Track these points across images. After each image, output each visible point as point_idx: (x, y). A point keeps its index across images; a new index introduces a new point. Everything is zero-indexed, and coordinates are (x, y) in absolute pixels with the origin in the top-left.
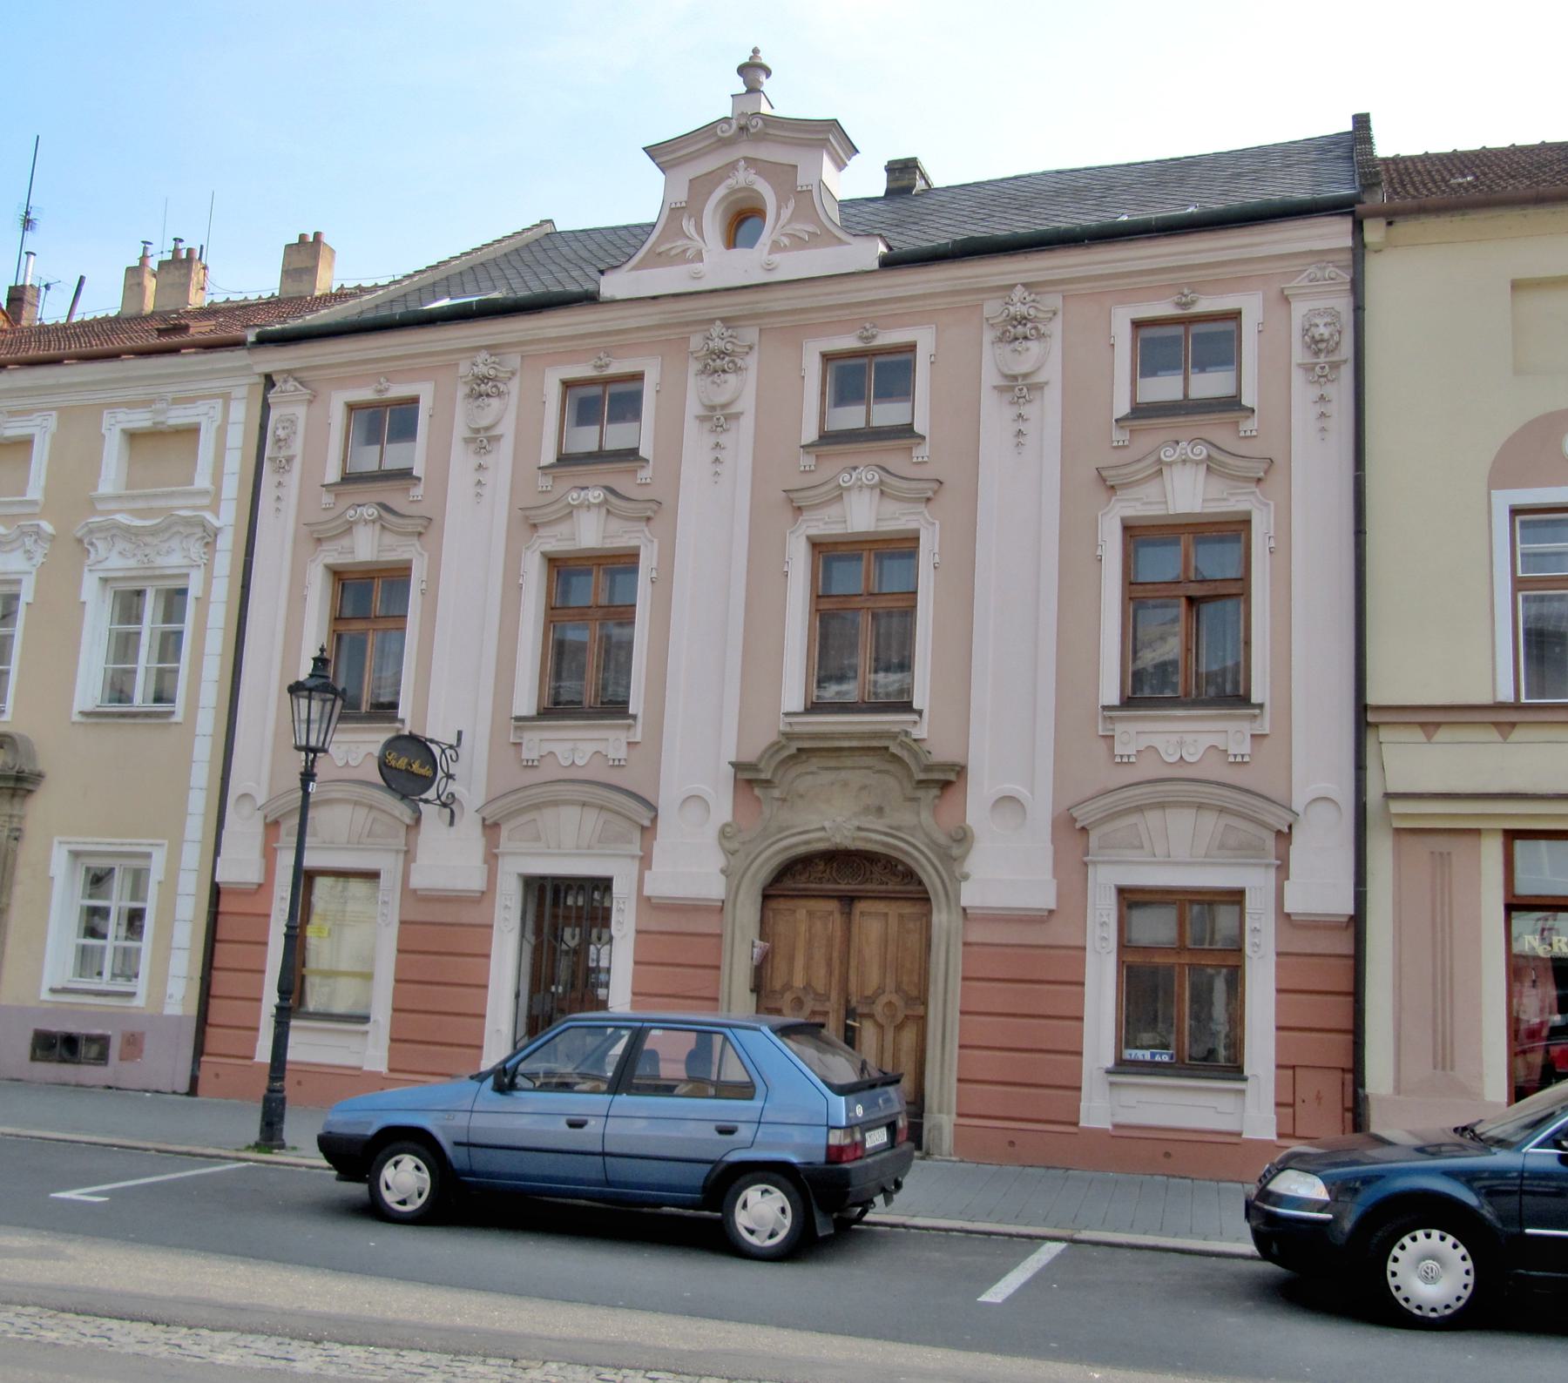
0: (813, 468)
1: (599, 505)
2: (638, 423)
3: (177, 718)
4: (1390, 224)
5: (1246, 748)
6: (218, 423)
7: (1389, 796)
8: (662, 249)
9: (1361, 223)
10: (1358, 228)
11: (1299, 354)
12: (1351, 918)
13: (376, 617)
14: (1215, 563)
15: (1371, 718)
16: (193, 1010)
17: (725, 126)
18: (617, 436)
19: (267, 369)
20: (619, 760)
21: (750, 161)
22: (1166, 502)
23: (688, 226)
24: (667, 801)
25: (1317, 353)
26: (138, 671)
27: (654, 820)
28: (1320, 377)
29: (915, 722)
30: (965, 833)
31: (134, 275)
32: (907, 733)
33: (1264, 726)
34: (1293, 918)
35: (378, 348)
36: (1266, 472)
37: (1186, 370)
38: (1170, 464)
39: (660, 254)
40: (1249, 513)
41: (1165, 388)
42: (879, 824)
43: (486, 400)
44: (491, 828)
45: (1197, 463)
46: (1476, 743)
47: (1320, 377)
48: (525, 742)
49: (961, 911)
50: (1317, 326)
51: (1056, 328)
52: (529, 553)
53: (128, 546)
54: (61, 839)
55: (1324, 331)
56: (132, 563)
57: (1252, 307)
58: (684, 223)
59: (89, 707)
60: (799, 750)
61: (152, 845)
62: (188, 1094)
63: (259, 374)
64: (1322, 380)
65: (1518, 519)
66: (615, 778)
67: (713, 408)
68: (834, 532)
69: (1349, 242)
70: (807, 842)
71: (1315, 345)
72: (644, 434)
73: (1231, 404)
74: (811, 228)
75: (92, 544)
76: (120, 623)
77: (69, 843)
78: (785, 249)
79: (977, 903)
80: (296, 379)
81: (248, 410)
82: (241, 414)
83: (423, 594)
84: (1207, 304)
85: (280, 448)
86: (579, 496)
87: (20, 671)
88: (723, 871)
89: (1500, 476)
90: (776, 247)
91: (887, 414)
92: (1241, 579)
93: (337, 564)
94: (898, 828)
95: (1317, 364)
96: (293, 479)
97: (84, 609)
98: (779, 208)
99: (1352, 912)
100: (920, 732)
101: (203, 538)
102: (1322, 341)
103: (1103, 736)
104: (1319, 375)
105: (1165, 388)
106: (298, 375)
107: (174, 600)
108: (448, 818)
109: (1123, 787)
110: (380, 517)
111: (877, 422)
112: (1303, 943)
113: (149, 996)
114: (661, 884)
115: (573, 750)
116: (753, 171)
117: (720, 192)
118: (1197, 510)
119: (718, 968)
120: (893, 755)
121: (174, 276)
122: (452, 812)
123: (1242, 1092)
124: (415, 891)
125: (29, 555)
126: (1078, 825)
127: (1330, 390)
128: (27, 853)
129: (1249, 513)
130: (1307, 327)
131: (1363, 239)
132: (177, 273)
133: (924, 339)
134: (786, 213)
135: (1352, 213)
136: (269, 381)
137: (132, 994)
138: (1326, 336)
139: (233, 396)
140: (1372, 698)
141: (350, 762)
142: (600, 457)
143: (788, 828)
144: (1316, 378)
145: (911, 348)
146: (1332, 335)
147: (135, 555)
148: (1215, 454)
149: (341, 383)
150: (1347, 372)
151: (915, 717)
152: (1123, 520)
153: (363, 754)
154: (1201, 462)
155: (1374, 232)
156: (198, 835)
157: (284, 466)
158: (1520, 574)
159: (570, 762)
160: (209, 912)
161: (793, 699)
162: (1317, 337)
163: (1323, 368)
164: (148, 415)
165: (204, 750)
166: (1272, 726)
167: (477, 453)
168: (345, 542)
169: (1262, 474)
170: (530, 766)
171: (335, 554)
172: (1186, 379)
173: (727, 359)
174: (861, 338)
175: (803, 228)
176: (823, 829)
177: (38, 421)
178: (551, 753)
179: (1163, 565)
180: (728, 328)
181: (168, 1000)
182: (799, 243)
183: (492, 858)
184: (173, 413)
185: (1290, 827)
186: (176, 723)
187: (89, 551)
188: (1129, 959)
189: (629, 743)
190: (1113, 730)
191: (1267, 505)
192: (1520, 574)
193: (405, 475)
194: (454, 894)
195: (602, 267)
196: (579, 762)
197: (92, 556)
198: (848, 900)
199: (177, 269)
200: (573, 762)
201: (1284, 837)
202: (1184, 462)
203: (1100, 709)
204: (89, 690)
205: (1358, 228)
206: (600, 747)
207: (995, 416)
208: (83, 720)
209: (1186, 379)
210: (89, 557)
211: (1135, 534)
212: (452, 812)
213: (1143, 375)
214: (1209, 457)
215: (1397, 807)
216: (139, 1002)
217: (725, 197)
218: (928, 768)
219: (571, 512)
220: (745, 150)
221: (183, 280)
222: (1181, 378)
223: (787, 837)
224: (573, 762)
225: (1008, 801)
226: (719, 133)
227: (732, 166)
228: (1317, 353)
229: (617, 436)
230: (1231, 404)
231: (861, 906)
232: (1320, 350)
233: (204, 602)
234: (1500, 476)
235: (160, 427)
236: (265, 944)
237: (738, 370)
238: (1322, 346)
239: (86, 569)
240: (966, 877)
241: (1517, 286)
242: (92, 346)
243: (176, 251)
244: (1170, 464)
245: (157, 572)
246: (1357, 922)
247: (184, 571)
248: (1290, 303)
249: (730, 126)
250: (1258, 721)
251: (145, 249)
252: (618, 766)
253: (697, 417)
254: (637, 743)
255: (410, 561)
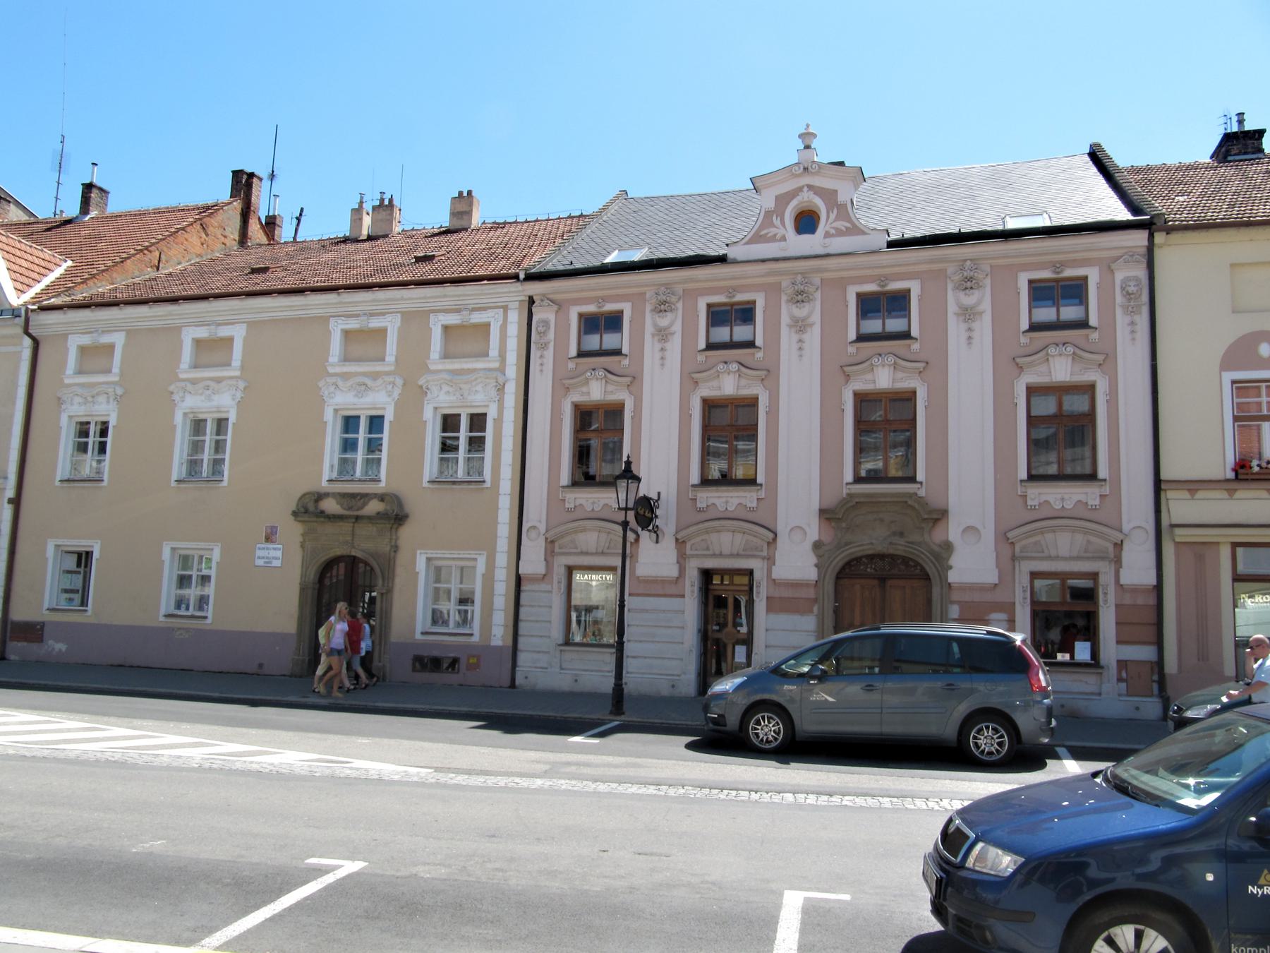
0: (1097, 340)
1: (735, 372)
2: (620, 335)
3: (488, 484)
4: (1167, 234)
5: (754, 504)
6: (501, 322)
7: (1173, 526)
8: (763, 233)
9: (1153, 234)
10: (1151, 236)
11: (1119, 299)
12: (1155, 586)
13: (602, 430)
14: (1076, 404)
15: (1163, 486)
16: (510, 642)
17: (797, 168)
18: (741, 333)
19: (530, 293)
20: (1096, 506)
21: (810, 187)
22: (1051, 376)
23: (777, 221)
24: (781, 528)
25: (1129, 300)
26: (382, 460)
27: (775, 539)
28: (1131, 312)
29: (919, 488)
30: (949, 546)
31: (357, 213)
32: (916, 494)
33: (762, 494)
34: (777, 581)
35: (1077, 252)
36: (631, 383)
37: (732, 324)
38: (1053, 356)
39: (761, 236)
40: (1095, 382)
41: (873, 326)
42: (902, 541)
43: (664, 314)
44: (680, 543)
45: (1068, 355)
46: (1214, 499)
47: (1131, 312)
48: (698, 498)
49: (947, 585)
50: (1130, 286)
51: (680, 305)
52: (846, 390)
53: (451, 390)
54: (422, 551)
55: (1132, 289)
56: (453, 398)
57: (1093, 276)
58: (774, 218)
59: (433, 478)
60: (857, 503)
61: (476, 554)
62: (510, 687)
63: (525, 296)
64: (1132, 314)
65: (1234, 386)
66: (750, 517)
67: (797, 321)
68: (870, 388)
69: (1146, 243)
70: (863, 550)
71: (1128, 295)
72: (624, 340)
73: (1083, 324)
74: (848, 225)
75: (428, 389)
76: (344, 433)
77: (426, 553)
78: (833, 236)
79: (1129, 583)
80: (548, 299)
81: (519, 315)
82: (515, 319)
83: (767, 414)
84: (1069, 273)
85: (541, 337)
86: (724, 367)
87: (231, 459)
88: (816, 565)
89: (1227, 364)
90: (827, 235)
91: (894, 325)
92: (1089, 415)
93: (579, 402)
94: (912, 543)
95: (1130, 305)
96: (549, 354)
97: (326, 425)
98: (828, 213)
99: (1155, 583)
100: (922, 493)
101: (497, 386)
102: (1132, 294)
103: (691, 499)
104: (1130, 311)
105: (873, 326)
106: (550, 296)
107: (478, 421)
108: (655, 539)
109: (716, 519)
110: (739, 370)
111: (736, 338)
112: (1127, 600)
113: (481, 635)
114: (780, 572)
115: (727, 502)
116: (812, 193)
117: (794, 203)
118: (1068, 379)
119: (551, 607)
120: (910, 506)
121: (383, 214)
122: (657, 535)
123: (1101, 673)
124: (638, 577)
125: (390, 394)
126: (1010, 541)
127: (1137, 318)
128: (402, 559)
129: (1095, 382)
130: (1124, 286)
131: (1153, 241)
132: (384, 213)
133: (915, 288)
134: (832, 216)
135: (1150, 229)
136: (531, 301)
137: (472, 635)
138: (1135, 291)
139: (509, 307)
140: (1163, 476)
141: (728, 508)
142: (731, 345)
143: (851, 543)
144: (1129, 312)
145: (1085, 279)
146: (1137, 291)
147: (454, 395)
148: (1078, 351)
149: (577, 302)
150: (1145, 310)
151: (919, 486)
152: (1027, 384)
153: (601, 505)
154: (892, 365)
155: (1159, 238)
156: (505, 548)
157: (544, 346)
158: (1235, 414)
159: (725, 509)
160: (515, 590)
161: (849, 476)
162: (1130, 292)
163: (1133, 308)
164: (459, 317)
165: (506, 504)
166: (1110, 490)
167: (797, 332)
168: (584, 389)
169: (1102, 362)
170: (701, 511)
171: (861, 384)
172: (601, 337)
173: (667, 305)
174: (879, 285)
175: (842, 225)
176: (872, 544)
177: (389, 319)
178: (714, 504)
179: (1046, 407)
180: (667, 288)
181: (492, 637)
182: (840, 233)
183: (682, 558)
184: (472, 316)
185: (1122, 541)
186: (487, 488)
187: (426, 392)
188: (1037, 608)
189: (1100, 495)
190: (1026, 492)
191: (924, 385)
192: (1235, 414)
193: (617, 352)
194: (1134, 587)
195: (728, 242)
196: (596, 509)
197: (429, 394)
198: (883, 580)
199: (384, 210)
200: (726, 509)
201: (1119, 546)
202: (1061, 355)
203: (1019, 483)
204: (178, 468)
205: (1151, 236)
206: (743, 501)
207: (955, 329)
208: (431, 486)
209: (601, 337)
210: (426, 396)
211: (1032, 391)
212: (657, 535)
213: (713, 326)
214: (1074, 353)
215: (1178, 531)
216: (476, 639)
217: (794, 207)
218: (930, 512)
219: (719, 376)
220: (807, 180)
221: (388, 217)
222: (881, 321)
223: (850, 548)
224: (726, 509)
225: (970, 529)
226: (793, 171)
227: (800, 189)
228: (1129, 300)
229: (610, 340)
230: (906, 335)
231: (889, 583)
232: (1131, 298)
233: (499, 421)
234: (1227, 364)
235: (465, 323)
236: (1117, 623)
237: (979, 287)
238: (1132, 296)
239: (426, 402)
240: (951, 568)
241: (1233, 265)
242: (155, 294)
243: (382, 200)
244: (1053, 356)
245: (469, 404)
246: (1159, 588)
247: (486, 404)
248: (1114, 273)
249: (799, 168)
250: (1104, 487)
251: (362, 198)
252: (752, 510)
253: (788, 325)
254: (1106, 495)
255: (624, 400)
